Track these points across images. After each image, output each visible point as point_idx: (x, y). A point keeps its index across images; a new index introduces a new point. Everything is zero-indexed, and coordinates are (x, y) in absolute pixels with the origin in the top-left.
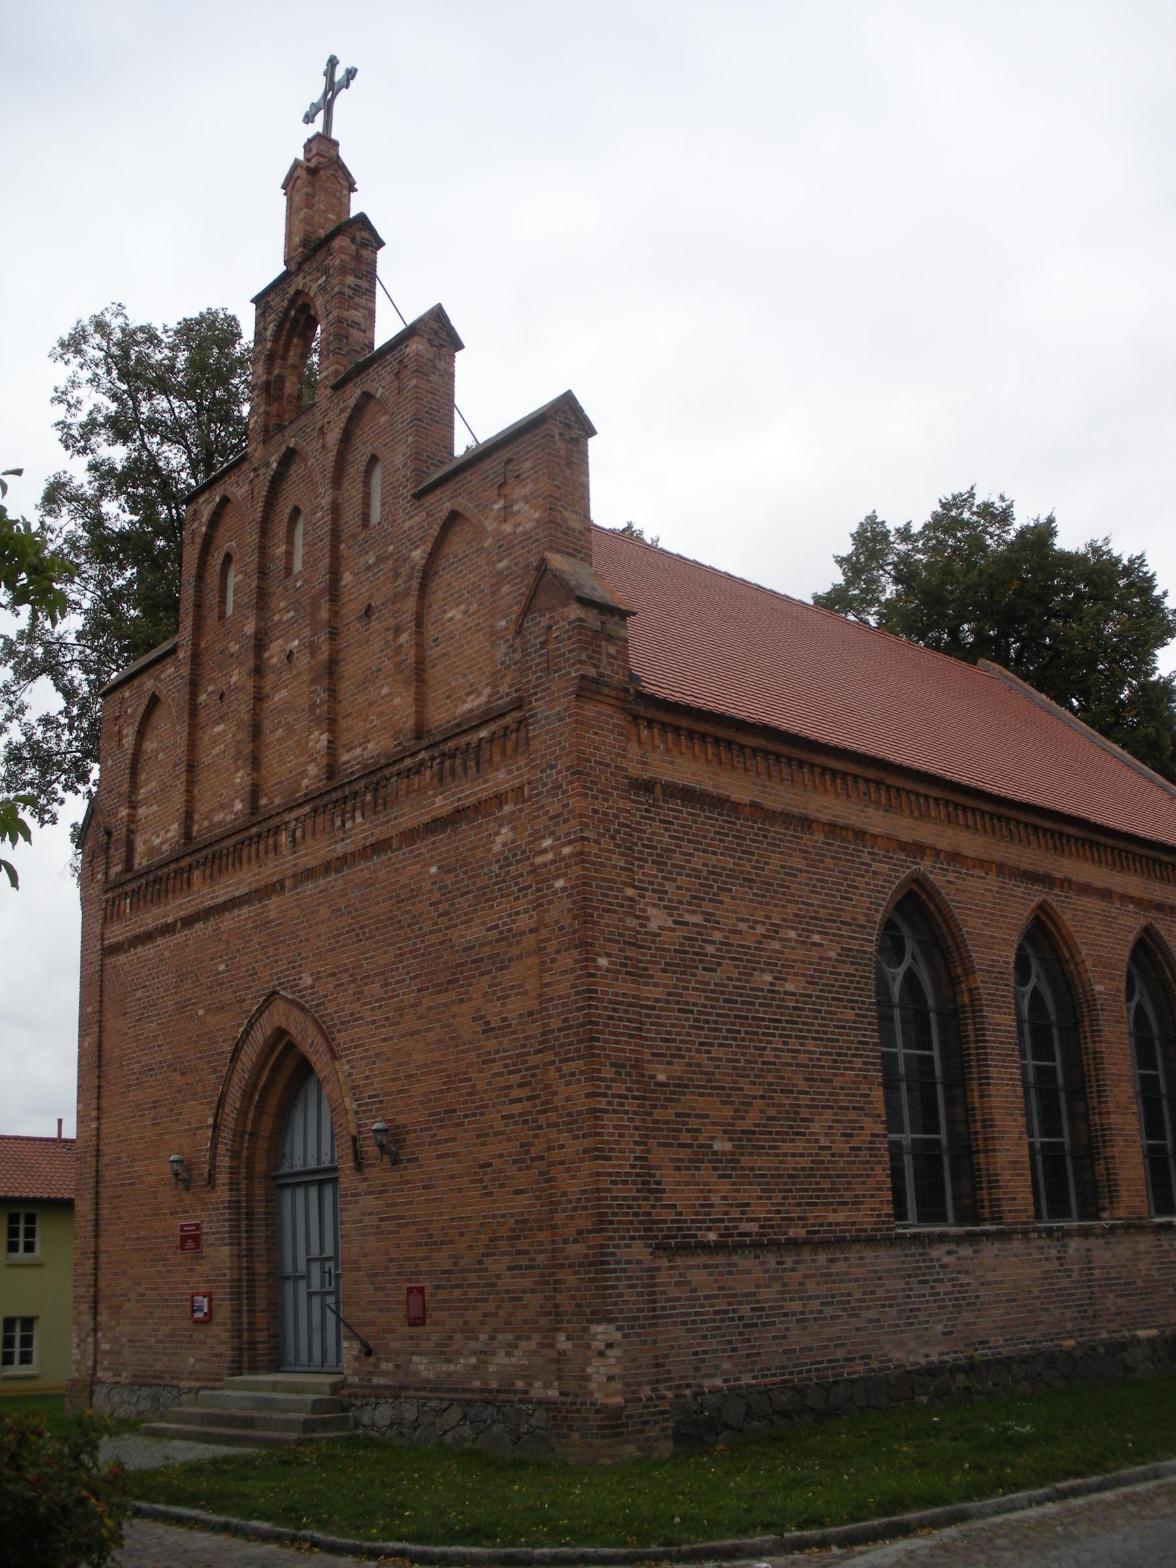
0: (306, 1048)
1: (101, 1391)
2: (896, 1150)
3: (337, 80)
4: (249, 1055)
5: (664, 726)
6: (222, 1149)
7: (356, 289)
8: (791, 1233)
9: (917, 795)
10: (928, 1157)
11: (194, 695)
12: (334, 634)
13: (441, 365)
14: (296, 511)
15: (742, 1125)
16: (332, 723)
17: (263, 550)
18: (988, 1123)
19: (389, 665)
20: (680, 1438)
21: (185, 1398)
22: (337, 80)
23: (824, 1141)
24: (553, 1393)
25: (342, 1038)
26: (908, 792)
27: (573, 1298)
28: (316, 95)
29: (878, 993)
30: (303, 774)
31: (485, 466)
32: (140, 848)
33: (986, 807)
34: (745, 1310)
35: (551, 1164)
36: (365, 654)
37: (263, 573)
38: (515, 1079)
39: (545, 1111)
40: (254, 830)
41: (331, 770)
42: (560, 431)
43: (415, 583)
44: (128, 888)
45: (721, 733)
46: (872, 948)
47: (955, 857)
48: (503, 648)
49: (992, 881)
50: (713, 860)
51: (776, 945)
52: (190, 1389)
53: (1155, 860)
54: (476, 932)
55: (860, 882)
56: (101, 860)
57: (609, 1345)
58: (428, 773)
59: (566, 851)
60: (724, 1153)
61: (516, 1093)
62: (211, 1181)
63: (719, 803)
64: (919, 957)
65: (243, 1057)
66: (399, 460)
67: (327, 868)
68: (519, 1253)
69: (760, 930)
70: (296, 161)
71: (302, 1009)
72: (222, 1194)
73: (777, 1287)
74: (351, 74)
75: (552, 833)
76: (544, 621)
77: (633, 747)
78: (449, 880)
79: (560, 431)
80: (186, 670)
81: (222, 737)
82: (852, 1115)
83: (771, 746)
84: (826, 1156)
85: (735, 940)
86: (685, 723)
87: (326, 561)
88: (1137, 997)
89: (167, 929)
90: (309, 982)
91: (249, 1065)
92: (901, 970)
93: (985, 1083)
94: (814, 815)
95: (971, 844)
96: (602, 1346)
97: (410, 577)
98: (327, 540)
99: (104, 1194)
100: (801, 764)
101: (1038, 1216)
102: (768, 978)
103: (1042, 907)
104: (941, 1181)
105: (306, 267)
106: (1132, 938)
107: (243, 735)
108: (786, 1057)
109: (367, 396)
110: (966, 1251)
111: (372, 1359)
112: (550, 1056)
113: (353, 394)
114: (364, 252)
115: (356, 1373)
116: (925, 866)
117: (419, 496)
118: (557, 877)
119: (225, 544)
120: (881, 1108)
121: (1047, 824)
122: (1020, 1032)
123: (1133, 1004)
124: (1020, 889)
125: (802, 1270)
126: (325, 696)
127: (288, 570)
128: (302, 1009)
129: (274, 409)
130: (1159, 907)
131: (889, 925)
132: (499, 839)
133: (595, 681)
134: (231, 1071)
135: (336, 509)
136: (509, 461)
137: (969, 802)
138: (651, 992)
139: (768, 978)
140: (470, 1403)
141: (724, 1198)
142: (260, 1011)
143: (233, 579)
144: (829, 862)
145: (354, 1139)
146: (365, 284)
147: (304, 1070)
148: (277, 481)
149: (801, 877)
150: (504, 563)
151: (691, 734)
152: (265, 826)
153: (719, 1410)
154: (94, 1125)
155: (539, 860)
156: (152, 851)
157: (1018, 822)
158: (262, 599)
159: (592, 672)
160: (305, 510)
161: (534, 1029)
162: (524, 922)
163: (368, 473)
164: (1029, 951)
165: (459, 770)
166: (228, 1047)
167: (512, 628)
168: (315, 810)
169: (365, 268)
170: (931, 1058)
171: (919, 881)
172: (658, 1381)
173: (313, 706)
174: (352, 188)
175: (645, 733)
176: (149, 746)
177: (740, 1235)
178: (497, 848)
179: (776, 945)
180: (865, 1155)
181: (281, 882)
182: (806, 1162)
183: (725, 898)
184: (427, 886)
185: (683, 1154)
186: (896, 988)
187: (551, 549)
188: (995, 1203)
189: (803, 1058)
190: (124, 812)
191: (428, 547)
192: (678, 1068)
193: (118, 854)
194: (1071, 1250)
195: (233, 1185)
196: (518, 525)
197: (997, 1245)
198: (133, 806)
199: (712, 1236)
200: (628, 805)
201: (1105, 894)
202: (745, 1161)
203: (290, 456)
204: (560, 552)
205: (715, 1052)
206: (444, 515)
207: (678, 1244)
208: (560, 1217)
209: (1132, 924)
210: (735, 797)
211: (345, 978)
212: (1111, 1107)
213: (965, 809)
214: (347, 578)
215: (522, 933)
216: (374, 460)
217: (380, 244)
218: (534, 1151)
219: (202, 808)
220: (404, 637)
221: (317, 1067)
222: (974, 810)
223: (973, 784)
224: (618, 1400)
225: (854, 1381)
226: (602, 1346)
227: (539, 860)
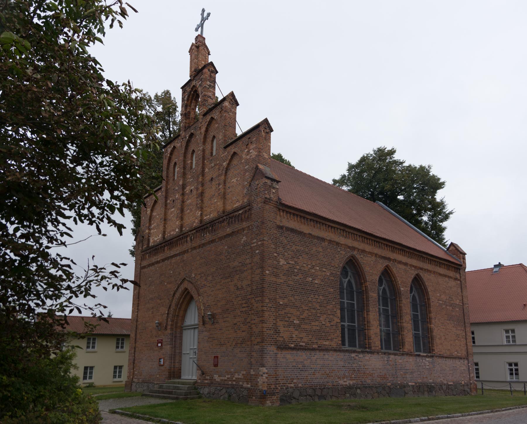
0: (192, 293)
1: (134, 384)
2: (343, 327)
3: (205, 17)
4: (178, 295)
5: (287, 212)
6: (169, 320)
7: (210, 86)
8: (314, 346)
9: (354, 234)
10: (352, 330)
11: (166, 201)
12: (203, 185)
13: (233, 110)
14: (194, 151)
15: (302, 317)
16: (202, 209)
17: (184, 161)
18: (368, 322)
19: (217, 194)
20: (282, 400)
21: (156, 386)
22: (205, 17)
23: (323, 323)
24: (249, 386)
25: (201, 291)
26: (352, 233)
27: (255, 360)
28: (199, 22)
29: (340, 285)
30: (194, 222)
31: (243, 139)
32: (151, 241)
33: (373, 238)
34: (300, 366)
35: (252, 324)
36: (211, 190)
37: (184, 168)
38: (244, 301)
39: (250, 310)
40: (181, 237)
41: (201, 221)
42: (264, 128)
43: (224, 172)
44: (148, 251)
45: (302, 214)
46: (339, 273)
47: (363, 251)
48: (246, 190)
49: (373, 258)
50: (298, 248)
51: (313, 271)
52: (157, 384)
53: (421, 256)
54: (236, 263)
55: (337, 256)
56: (141, 245)
57: (264, 373)
58: (226, 222)
59: (259, 243)
60: (297, 324)
61: (244, 305)
62: (166, 329)
63: (300, 233)
64: (352, 277)
65: (176, 295)
66: (221, 137)
67: (199, 246)
68: (242, 347)
69: (309, 266)
70: (193, 43)
71: (192, 283)
72: (169, 331)
73: (309, 361)
74: (209, 15)
75: (256, 238)
76: (257, 183)
77: (278, 217)
78: (230, 250)
79: (264, 128)
80: (164, 194)
81: (173, 212)
82: (331, 316)
83: (315, 219)
84: (324, 327)
85: (302, 268)
86: (292, 211)
87: (201, 165)
88: (413, 292)
89: (158, 262)
90: (194, 276)
91: (177, 297)
92: (347, 280)
93: (368, 311)
94: (325, 238)
95: (368, 248)
96: (262, 374)
97: (223, 170)
98: (201, 159)
99: (138, 332)
100: (323, 224)
101: (382, 348)
102: (311, 279)
103: (387, 266)
104: (354, 338)
105: (196, 78)
106: (413, 276)
107: (179, 211)
108: (314, 300)
109: (212, 118)
110: (361, 356)
111: (204, 376)
112: (253, 296)
113: (208, 118)
114: (212, 74)
115: (200, 379)
116: (355, 253)
117: (226, 147)
118: (257, 250)
119: (174, 160)
120: (339, 315)
121: (390, 244)
122: (379, 299)
123: (412, 294)
124: (381, 261)
125: (316, 357)
126: (200, 202)
127: (191, 167)
128: (192, 283)
129: (187, 121)
130: (421, 269)
131: (344, 268)
132: (243, 240)
133: (269, 199)
134: (173, 299)
135: (204, 151)
136: (249, 138)
137: (368, 237)
138: (279, 281)
139: (311, 279)
140: (228, 388)
141: (296, 336)
142: (181, 283)
143: (176, 170)
144: (329, 250)
145: (203, 317)
146: (212, 85)
147: (192, 298)
148: (188, 142)
149: (321, 254)
150: (247, 167)
151: (294, 214)
152: (184, 235)
153: (292, 393)
154: (136, 313)
155: (252, 245)
156: (154, 241)
157: (382, 243)
158: (184, 174)
159: (268, 196)
160: (196, 151)
161: (249, 289)
162: (248, 261)
163: (213, 141)
164: (383, 278)
165: (233, 222)
166: (172, 293)
167: (248, 184)
168: (197, 231)
169: (212, 79)
170: (354, 304)
171: (353, 257)
172: (277, 384)
173: (197, 204)
174: (209, 54)
175: (282, 214)
176: (154, 214)
177: (300, 346)
178: (242, 242)
179: (313, 271)
180: (334, 327)
181: (188, 250)
182: (318, 328)
183: (300, 257)
184: (224, 252)
185: (286, 323)
186: (345, 285)
187: (259, 163)
188: (369, 344)
189: (319, 301)
190: (147, 231)
191: (228, 162)
192: (286, 301)
193: (145, 243)
194: (391, 359)
195: (172, 329)
196: (251, 156)
197: (370, 355)
198: (150, 230)
199: (292, 346)
200: (276, 232)
201: (406, 264)
202: (302, 326)
203: (192, 135)
204: (262, 164)
205: (296, 297)
206: (232, 153)
207: (283, 347)
208: (253, 338)
209: (413, 273)
210: (305, 232)
211: (203, 275)
212: (404, 321)
213: (367, 239)
214: (207, 170)
215: (247, 264)
216: (214, 137)
217: (217, 72)
218: (248, 321)
219: (168, 230)
220: (221, 186)
221: (195, 298)
222: (370, 239)
223: (370, 232)
224: (265, 389)
225: (329, 388)
226: (262, 374)
227: (252, 245)
